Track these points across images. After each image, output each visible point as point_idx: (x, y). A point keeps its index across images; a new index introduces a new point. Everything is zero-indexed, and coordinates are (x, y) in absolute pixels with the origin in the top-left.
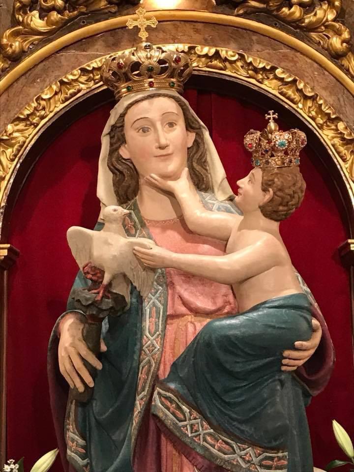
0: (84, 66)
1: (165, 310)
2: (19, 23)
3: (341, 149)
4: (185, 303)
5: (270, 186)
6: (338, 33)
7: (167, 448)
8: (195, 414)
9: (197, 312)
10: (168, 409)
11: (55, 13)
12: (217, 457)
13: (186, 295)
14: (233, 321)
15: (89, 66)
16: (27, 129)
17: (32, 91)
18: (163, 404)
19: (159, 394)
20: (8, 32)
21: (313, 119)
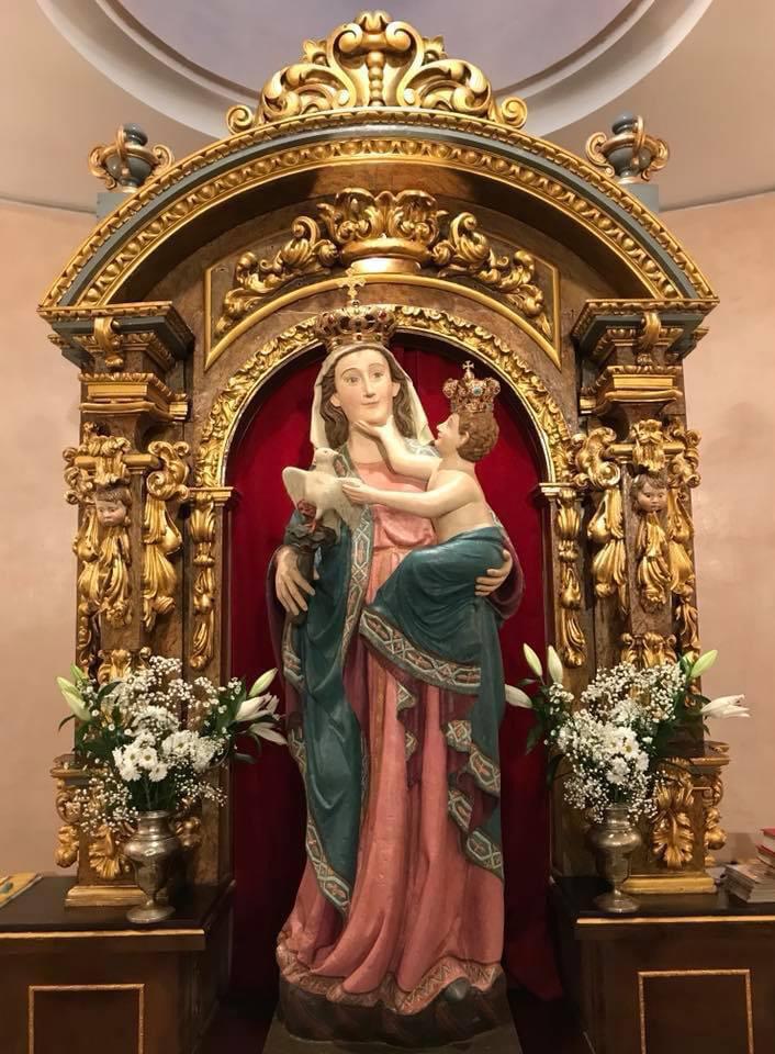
1: (372, 543)
3: (535, 401)
4: (390, 537)
5: (466, 429)
8: (398, 634)
9: (400, 544)
10: (374, 630)
12: (419, 672)
13: (391, 530)
17: (253, 347)
18: (368, 624)
19: (366, 616)
20: (230, 293)
21: (509, 373)
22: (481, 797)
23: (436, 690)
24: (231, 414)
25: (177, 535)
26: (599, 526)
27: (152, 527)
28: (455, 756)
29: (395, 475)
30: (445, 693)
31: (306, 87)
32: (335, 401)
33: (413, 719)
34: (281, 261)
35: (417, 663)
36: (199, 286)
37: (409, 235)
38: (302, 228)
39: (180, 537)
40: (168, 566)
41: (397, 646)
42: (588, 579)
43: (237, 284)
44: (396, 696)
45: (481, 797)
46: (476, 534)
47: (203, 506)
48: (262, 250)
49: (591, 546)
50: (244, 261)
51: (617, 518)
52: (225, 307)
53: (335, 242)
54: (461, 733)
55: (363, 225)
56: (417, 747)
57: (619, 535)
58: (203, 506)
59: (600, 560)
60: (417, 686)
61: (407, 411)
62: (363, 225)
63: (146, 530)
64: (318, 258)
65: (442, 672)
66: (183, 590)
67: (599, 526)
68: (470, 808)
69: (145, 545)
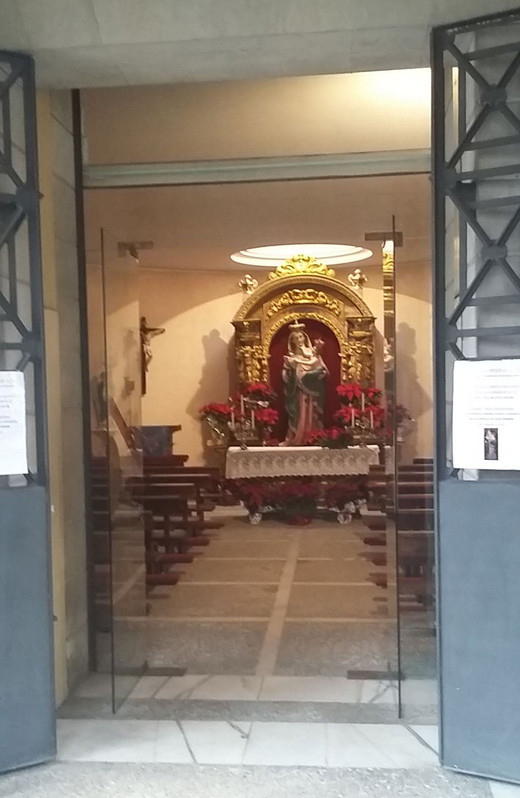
4: (303, 368)
7: (300, 392)
9: (305, 370)
22: (319, 414)
24: (270, 338)
26: (350, 363)
28: (314, 407)
29: (305, 356)
32: (293, 341)
33: (307, 401)
36: (261, 309)
41: (306, 390)
43: (271, 309)
44: (304, 397)
45: (319, 414)
48: (276, 300)
54: (316, 404)
60: (308, 395)
66: (261, 378)
68: (413, 596)
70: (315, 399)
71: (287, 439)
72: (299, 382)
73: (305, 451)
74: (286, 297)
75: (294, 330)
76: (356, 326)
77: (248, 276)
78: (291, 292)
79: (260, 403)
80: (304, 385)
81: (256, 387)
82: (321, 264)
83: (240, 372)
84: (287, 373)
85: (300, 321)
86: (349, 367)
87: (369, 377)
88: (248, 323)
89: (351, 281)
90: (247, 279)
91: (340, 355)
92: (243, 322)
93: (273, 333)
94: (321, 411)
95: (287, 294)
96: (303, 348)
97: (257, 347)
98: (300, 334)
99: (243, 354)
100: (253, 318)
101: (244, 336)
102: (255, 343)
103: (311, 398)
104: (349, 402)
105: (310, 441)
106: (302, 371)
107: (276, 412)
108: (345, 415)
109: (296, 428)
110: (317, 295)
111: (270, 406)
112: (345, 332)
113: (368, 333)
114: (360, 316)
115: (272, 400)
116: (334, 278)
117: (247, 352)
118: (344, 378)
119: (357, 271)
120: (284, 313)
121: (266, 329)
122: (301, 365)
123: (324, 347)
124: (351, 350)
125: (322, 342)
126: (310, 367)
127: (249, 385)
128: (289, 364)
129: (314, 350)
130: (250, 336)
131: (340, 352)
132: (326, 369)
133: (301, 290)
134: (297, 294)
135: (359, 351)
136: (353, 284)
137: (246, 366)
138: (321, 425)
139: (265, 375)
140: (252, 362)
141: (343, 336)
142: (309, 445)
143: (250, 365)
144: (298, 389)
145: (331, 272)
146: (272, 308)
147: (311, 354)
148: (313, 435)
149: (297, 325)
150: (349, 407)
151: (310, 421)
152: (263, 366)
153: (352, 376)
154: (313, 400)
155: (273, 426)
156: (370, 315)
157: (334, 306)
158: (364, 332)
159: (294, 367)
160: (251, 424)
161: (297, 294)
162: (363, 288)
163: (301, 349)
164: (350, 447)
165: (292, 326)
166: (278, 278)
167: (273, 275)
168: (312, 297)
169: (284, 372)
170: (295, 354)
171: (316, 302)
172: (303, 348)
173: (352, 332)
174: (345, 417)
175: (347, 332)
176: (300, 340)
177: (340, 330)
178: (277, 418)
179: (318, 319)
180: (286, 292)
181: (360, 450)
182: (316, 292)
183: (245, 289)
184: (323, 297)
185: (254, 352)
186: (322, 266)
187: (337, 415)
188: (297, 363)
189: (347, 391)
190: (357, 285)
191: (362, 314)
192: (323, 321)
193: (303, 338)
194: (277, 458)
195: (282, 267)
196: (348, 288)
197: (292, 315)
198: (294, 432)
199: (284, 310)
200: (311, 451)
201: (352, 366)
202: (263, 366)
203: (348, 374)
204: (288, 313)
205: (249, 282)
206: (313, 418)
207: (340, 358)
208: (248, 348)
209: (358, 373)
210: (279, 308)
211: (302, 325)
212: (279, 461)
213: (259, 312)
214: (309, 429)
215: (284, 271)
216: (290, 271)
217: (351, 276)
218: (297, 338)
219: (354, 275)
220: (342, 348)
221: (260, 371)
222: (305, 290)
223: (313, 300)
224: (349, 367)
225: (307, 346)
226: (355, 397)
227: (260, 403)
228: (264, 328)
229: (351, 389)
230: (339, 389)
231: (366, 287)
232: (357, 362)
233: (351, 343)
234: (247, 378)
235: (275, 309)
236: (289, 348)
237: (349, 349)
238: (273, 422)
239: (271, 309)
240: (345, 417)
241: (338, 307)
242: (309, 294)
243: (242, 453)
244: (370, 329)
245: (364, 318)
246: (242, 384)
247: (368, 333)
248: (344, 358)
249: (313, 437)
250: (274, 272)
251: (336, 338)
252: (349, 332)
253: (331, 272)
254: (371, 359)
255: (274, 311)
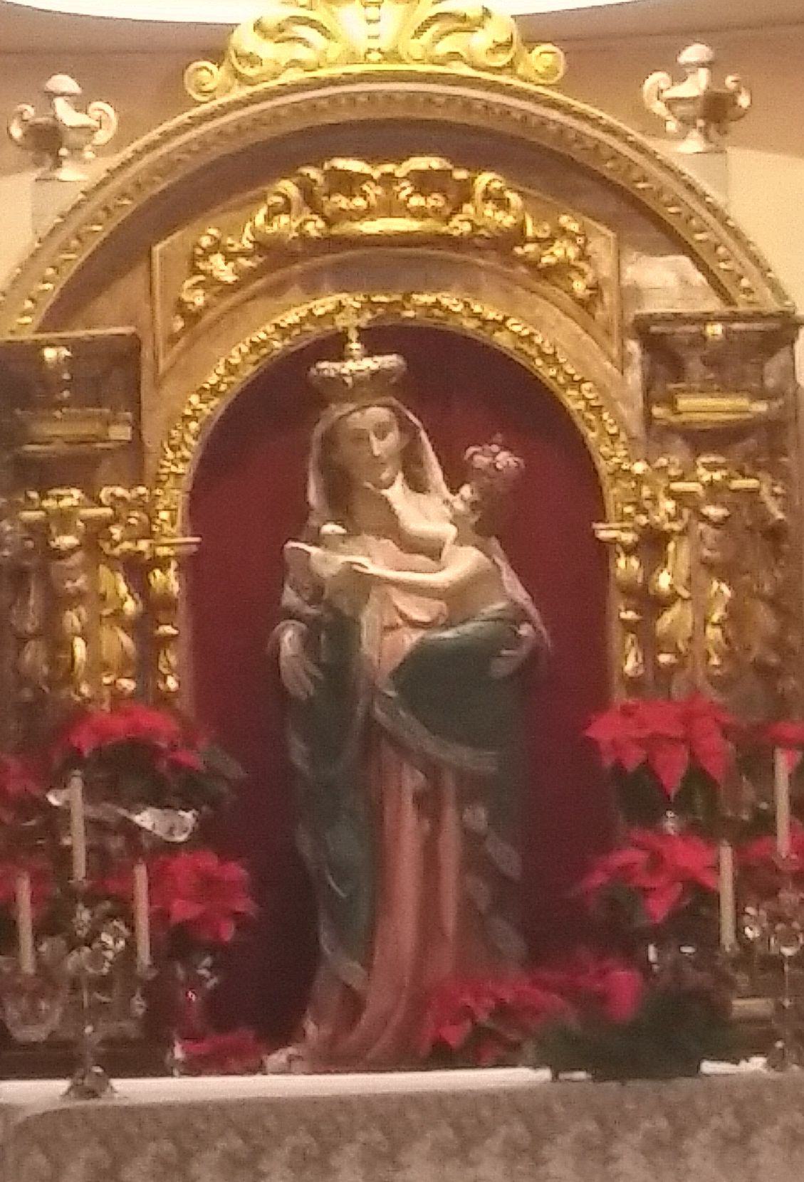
0: (277, 321)
2: (203, 273)
4: (402, 615)
6: (582, 274)
7: (388, 753)
9: (415, 625)
11: (465, 816)
13: (402, 607)
14: (448, 634)
15: (282, 321)
16: (213, 399)
17: (217, 351)
20: (188, 283)
23: (60, 503)
24: (191, 442)
25: (137, 603)
26: (664, 581)
27: (109, 593)
28: (471, 838)
29: (413, 546)
30: (462, 776)
31: (286, 34)
33: (428, 803)
34: (252, 238)
35: (431, 745)
37: (420, 214)
38: (279, 200)
39: (140, 604)
40: (126, 640)
42: (651, 644)
44: (412, 780)
46: (496, 615)
47: (162, 563)
48: (225, 219)
49: (654, 604)
50: (206, 241)
51: (684, 572)
52: (181, 304)
53: (324, 218)
54: (479, 817)
55: (359, 202)
56: (432, 829)
57: (685, 594)
58: (162, 563)
59: (666, 621)
60: (433, 770)
61: (420, 463)
62: (359, 202)
63: (103, 597)
64: (304, 237)
65: (460, 756)
67: (664, 581)
69: (101, 616)
70: (471, 790)
71: (311, 1028)
72: (374, 691)
73: (457, 1097)
74: (288, 200)
75: (338, 389)
76: (695, 366)
77: (64, 83)
78: (313, 173)
79: (146, 819)
80: (413, 709)
81: (120, 725)
82: (487, 13)
83: (22, 640)
84: (309, 642)
85: (375, 340)
86: (660, 604)
87: (773, 660)
88: (65, 352)
89: (659, 108)
90: (59, 102)
91: (605, 533)
92: (39, 346)
93: (212, 408)
94: (507, 858)
95: (288, 187)
96: (397, 494)
97: (120, 491)
98: (378, 414)
99: (40, 531)
100: (73, 329)
101: (48, 430)
102: (106, 466)
103: (449, 784)
104: (667, 804)
105: (456, 1036)
106: (393, 628)
107: (237, 871)
108: (645, 881)
109: (368, 966)
110: (464, 194)
111: (204, 834)
112: (628, 401)
113: (761, 407)
114: (713, 305)
115: (214, 802)
116: (557, 87)
117: (64, 519)
118: (630, 665)
119: (694, 53)
120: (276, 290)
121: (169, 389)
122: (386, 598)
123: (521, 485)
124: (669, 505)
125: (505, 459)
126: (438, 605)
127: (80, 714)
128: (317, 591)
129: (459, 506)
130: (85, 429)
131: (603, 519)
132: (533, 611)
133: (372, 159)
134: (349, 184)
135: (714, 512)
136: (672, 126)
137: (57, 602)
138: (512, 944)
139: (171, 658)
140: (95, 580)
141: (619, 421)
142: (443, 1057)
143: (80, 596)
144: (373, 734)
145: (544, 59)
146: (201, 265)
147: (450, 531)
148: (468, 1000)
149: (359, 364)
150: (665, 837)
151: (450, 922)
152: (155, 607)
153: (677, 653)
154: (465, 799)
155: (224, 956)
156: (773, 306)
157: (561, 251)
158: (742, 402)
159: (344, 604)
160: (131, 946)
161: (349, 184)
162: (729, 149)
163: (386, 502)
164: (708, 1067)
165: (328, 368)
166: (240, 93)
167: (210, 75)
168: (435, 201)
169: (289, 638)
170: (353, 532)
171: (459, 226)
172: (397, 494)
173: (671, 402)
174: (646, 892)
175: (640, 404)
176: (378, 447)
177: (601, 389)
178: (244, 905)
179: (470, 324)
180: (287, 167)
181: (777, 1086)
182: (461, 174)
183: (49, 161)
184: (503, 204)
185: (107, 523)
186: (489, 24)
187: (598, 879)
188: (361, 583)
189: (652, 743)
190: (695, 133)
191: (727, 299)
192: (502, 339)
193: (393, 438)
194: (362, 1136)
195: (258, 26)
196: (641, 149)
197: (324, 305)
198: (357, 985)
199: (276, 276)
200: (492, 1098)
201: (674, 597)
202: (155, 607)
203: (651, 644)
204: (295, 292)
205: (67, 114)
206: (467, 904)
207: (604, 551)
208: (73, 497)
209: (713, 633)
210: (245, 263)
211: (389, 361)
212: (514, 1152)
213: (131, 286)
214: (444, 963)
215: (269, 51)
216: (300, 52)
217: (657, 79)
218: (361, 438)
219: (679, 76)
220: (614, 493)
221: (141, 628)
222: (399, 161)
223: (447, 220)
224: (660, 604)
225: (417, 484)
226: (698, 776)
227: (146, 819)
228: (158, 384)
229: (678, 732)
230: (604, 730)
231: (743, 143)
232: (702, 576)
233: (673, 460)
234: (65, 673)
235: (222, 270)
236: (313, 495)
237: (654, 499)
238: (228, 933)
239: (196, 271)
240: (646, 892)
241: (584, 256)
242: (423, 182)
243: (84, 1112)
244: (770, 382)
245: (735, 317)
246: (31, 710)
247: (761, 407)
248: (630, 551)
249: (469, 1013)
250: (217, 54)
251: (581, 442)
252: (648, 400)
253: (544, 59)
254: (777, 554)
255: (210, 283)
